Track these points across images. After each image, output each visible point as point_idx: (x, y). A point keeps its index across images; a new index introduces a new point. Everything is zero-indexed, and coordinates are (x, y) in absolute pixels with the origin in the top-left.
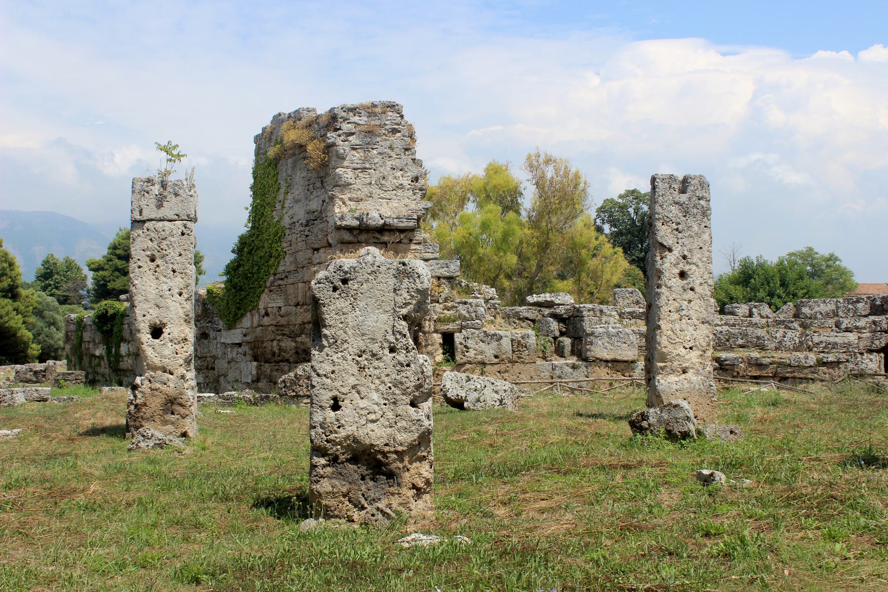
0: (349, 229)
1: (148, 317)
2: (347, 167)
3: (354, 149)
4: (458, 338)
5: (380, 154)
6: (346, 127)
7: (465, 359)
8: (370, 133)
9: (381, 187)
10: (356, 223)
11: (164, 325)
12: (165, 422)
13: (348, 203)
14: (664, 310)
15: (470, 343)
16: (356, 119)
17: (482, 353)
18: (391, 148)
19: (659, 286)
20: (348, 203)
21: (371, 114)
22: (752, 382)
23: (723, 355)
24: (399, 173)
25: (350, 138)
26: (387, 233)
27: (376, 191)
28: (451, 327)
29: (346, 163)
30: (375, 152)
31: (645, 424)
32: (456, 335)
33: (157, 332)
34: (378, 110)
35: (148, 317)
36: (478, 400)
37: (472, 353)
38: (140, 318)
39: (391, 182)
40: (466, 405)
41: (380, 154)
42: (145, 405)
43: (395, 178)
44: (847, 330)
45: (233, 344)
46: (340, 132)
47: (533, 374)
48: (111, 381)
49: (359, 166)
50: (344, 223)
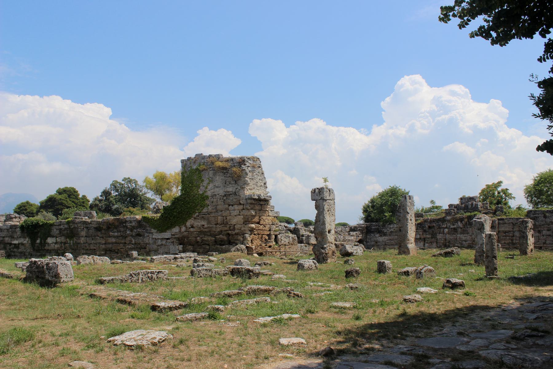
0: (254, 199)
1: (328, 228)
2: (248, 178)
3: (250, 172)
4: (279, 236)
5: (256, 174)
6: (248, 164)
7: (281, 244)
8: (254, 167)
9: (257, 185)
10: (257, 198)
11: (331, 230)
12: (332, 258)
13: (249, 190)
14: (409, 228)
15: (282, 238)
16: (250, 162)
17: (285, 242)
18: (259, 172)
19: (407, 222)
20: (249, 190)
21: (254, 161)
22: (390, 248)
23: (337, 243)
24: (261, 181)
25: (249, 168)
26: (262, 201)
27: (255, 186)
28: (278, 233)
29: (248, 177)
30: (255, 173)
31: (453, 252)
32: (279, 236)
33: (329, 232)
34: (255, 159)
35: (328, 228)
36: (357, 253)
37: (283, 242)
38: (327, 228)
39: (259, 184)
40: (354, 254)
41: (256, 174)
42: (328, 253)
43: (260, 183)
44: (352, 236)
45: (162, 239)
46: (246, 166)
47: (297, 248)
48: (144, 254)
49: (251, 178)
50: (255, 197)
